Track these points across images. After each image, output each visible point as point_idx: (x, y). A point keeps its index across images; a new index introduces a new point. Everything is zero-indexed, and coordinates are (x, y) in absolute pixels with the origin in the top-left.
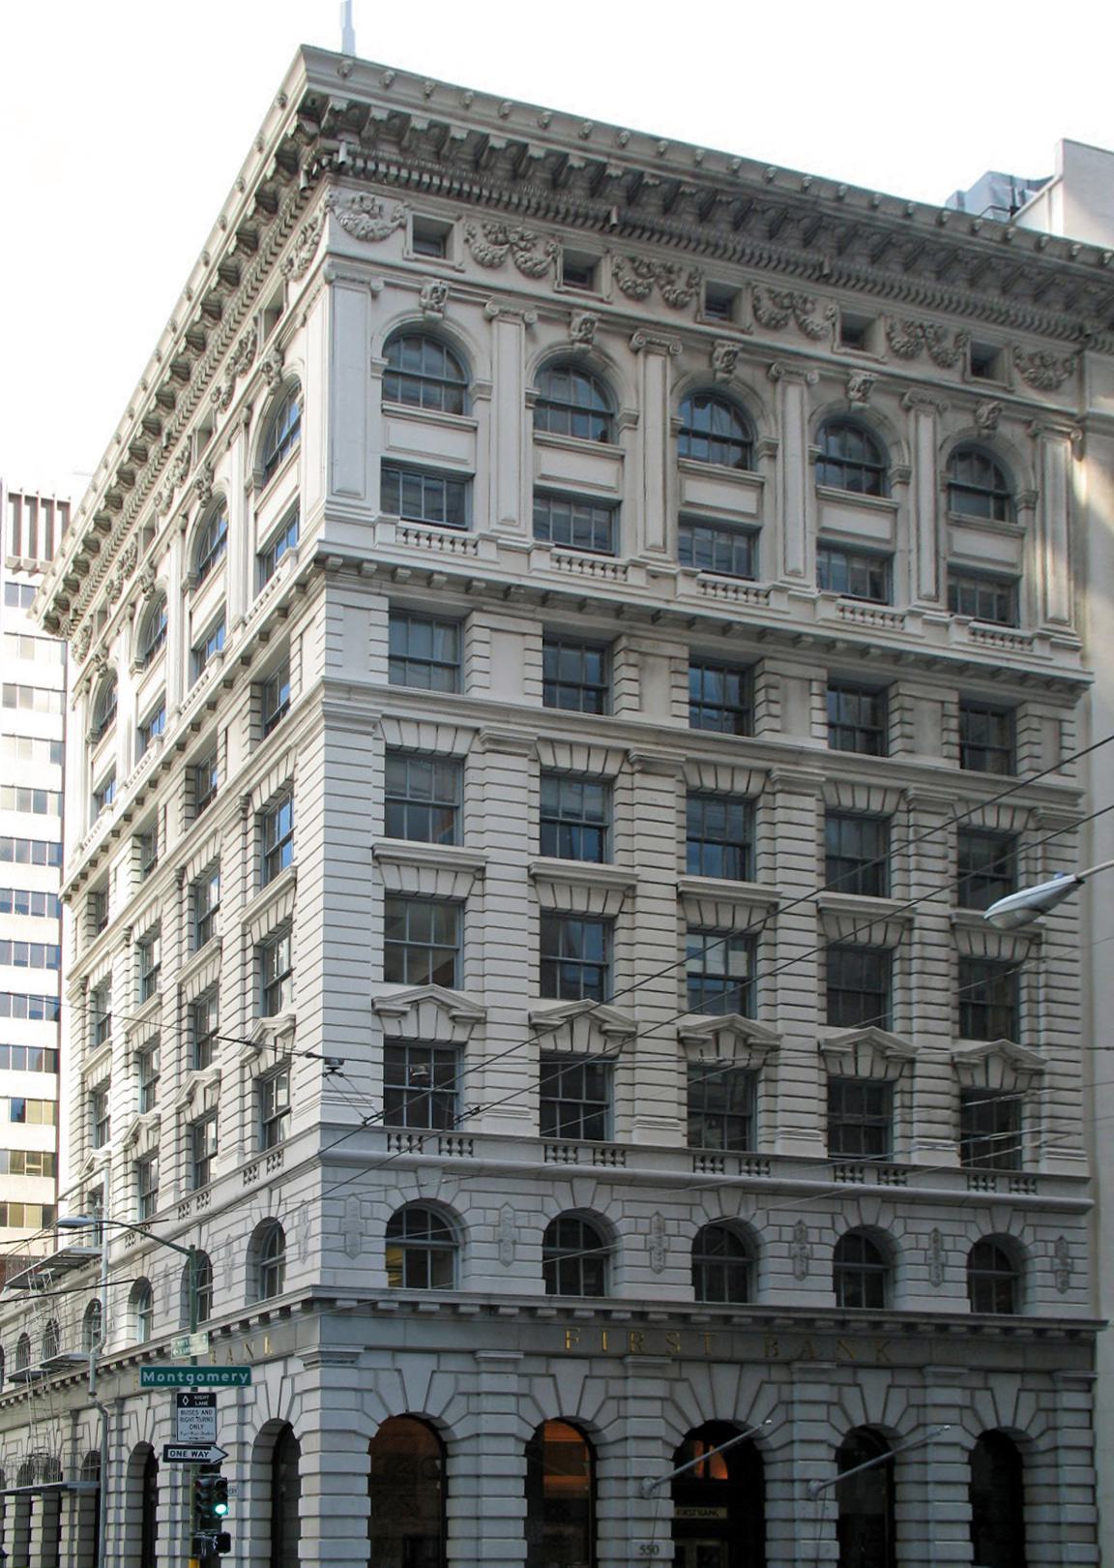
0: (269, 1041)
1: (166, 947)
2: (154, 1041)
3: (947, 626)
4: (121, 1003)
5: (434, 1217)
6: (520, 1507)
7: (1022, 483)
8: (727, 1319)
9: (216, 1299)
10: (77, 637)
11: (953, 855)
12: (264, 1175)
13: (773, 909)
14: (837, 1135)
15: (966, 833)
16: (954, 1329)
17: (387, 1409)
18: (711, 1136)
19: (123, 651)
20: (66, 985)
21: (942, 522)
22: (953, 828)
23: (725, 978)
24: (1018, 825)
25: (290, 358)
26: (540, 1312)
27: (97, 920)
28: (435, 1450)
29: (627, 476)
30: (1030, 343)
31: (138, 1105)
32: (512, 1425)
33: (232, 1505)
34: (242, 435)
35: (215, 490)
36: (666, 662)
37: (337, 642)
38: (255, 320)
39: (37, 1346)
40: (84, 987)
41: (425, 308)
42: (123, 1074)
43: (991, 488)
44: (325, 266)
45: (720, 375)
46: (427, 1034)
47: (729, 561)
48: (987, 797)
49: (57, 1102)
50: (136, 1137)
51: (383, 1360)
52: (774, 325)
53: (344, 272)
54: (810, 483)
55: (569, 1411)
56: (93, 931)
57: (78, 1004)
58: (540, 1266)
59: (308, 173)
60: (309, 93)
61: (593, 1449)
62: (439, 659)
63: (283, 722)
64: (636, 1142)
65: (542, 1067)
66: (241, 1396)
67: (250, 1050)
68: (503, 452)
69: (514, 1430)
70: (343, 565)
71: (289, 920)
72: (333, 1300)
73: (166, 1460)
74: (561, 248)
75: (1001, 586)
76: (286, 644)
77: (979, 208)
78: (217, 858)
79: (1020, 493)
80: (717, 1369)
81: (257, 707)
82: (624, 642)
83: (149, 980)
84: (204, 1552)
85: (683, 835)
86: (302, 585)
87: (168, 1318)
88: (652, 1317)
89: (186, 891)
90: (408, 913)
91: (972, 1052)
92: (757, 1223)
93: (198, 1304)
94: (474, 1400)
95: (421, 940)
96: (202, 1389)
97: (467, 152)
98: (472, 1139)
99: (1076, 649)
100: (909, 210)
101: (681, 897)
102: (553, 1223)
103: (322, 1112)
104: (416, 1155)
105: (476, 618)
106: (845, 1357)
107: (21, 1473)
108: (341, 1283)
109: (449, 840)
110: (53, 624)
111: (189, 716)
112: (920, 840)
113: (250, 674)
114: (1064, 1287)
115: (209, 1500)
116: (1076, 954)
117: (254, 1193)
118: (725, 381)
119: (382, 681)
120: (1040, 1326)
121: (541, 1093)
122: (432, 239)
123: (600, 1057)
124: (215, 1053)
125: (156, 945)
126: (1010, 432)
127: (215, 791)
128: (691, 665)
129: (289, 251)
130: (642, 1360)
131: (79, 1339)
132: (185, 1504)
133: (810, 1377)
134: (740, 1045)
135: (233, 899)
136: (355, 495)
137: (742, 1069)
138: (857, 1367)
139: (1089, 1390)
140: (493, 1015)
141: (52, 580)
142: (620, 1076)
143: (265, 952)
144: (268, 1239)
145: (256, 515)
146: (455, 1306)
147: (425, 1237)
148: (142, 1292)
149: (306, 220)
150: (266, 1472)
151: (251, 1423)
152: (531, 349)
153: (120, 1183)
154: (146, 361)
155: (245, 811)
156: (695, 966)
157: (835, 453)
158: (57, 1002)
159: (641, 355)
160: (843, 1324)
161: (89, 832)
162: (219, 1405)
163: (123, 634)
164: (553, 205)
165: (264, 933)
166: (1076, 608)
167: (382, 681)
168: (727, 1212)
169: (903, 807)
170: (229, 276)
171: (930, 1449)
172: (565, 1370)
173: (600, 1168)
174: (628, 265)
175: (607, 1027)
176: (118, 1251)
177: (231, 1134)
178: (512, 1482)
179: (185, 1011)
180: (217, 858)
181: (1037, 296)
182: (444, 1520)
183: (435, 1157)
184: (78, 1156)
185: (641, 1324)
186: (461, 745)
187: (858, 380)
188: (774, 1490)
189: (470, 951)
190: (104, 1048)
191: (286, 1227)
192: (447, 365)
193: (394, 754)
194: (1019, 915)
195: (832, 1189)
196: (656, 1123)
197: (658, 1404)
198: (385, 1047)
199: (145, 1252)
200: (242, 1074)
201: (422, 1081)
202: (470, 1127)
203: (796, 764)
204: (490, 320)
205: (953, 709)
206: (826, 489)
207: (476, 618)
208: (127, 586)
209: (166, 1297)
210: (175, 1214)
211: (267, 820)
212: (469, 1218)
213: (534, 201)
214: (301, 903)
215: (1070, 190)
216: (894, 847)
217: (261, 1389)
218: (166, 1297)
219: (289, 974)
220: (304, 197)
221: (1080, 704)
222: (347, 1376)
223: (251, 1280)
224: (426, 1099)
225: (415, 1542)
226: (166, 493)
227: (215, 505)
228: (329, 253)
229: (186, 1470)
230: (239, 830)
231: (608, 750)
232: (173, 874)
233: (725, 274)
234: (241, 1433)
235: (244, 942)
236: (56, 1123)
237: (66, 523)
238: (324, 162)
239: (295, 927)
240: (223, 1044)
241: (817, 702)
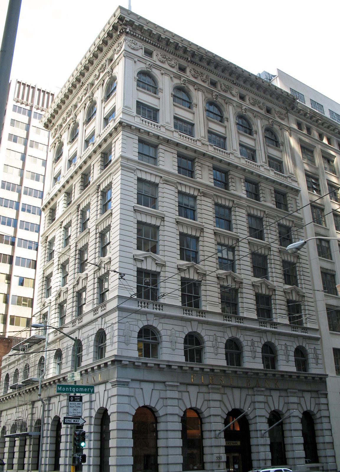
0: (103, 265)
1: (73, 230)
2: (67, 262)
3: (269, 170)
4: (58, 247)
5: (152, 332)
6: (180, 443)
7: (280, 140)
8: (236, 372)
9: (84, 358)
10: (53, 131)
11: (277, 231)
12: (100, 313)
13: (238, 240)
14: (259, 311)
15: (280, 225)
16: (293, 377)
17: (138, 404)
18: (227, 309)
19: (66, 137)
20: (41, 238)
21: (265, 145)
22: (276, 223)
23: (228, 260)
24: (291, 225)
25: (114, 71)
26: (184, 368)
27: (52, 218)
28: (153, 420)
29: (195, 118)
30: (278, 109)
31: (61, 283)
32: (176, 410)
33: (87, 442)
34: (101, 87)
35: (94, 99)
36: (207, 167)
37: (125, 146)
38: (106, 60)
39: (21, 374)
40: (46, 240)
41: (147, 68)
42: (57, 272)
43: (274, 139)
44: (123, 52)
45: (214, 99)
46: (149, 268)
47: (220, 144)
48: (283, 216)
49: (34, 280)
50: (59, 295)
51: (136, 385)
52: (225, 91)
53: (128, 55)
54: (236, 129)
55: (194, 406)
56: (50, 221)
57: (44, 246)
58: (183, 351)
59: (120, 32)
60: (120, 15)
61: (201, 419)
62: (151, 155)
63: (109, 165)
64: (208, 310)
65: (182, 283)
66: (91, 397)
67: (97, 268)
68: (167, 108)
69: (177, 412)
70: (126, 125)
71: (110, 225)
72: (121, 361)
73: (64, 423)
74: (178, 62)
75: (279, 163)
76: (111, 144)
77: (263, 77)
78: (89, 203)
79: (280, 142)
80: (234, 389)
81: (103, 160)
82: (197, 160)
83: (67, 240)
84: (77, 462)
85: (214, 216)
86: (116, 129)
87: (67, 367)
88: (215, 371)
89: (80, 212)
90: (144, 228)
91: (288, 289)
92: (241, 339)
93: (77, 360)
94: (165, 400)
95: (147, 237)
96: (78, 394)
97: (156, 37)
98: (163, 305)
99: (296, 182)
100: (250, 75)
101: (215, 234)
102: (186, 336)
103: (119, 292)
104: (146, 309)
105: (160, 146)
106: (267, 386)
107: (12, 428)
108: (124, 354)
109: (154, 207)
110: (46, 126)
111: (83, 159)
112: (270, 226)
113: (101, 150)
114: (317, 364)
115: (79, 440)
116: (307, 263)
117: (96, 319)
118: (215, 101)
119: (136, 159)
120: (313, 376)
121: (182, 291)
122: (149, 53)
123: (197, 281)
124: (86, 268)
125: (70, 228)
126: (276, 127)
127: (90, 182)
128: (213, 169)
129: (115, 47)
130: (214, 386)
131: (36, 372)
132: (71, 442)
133: (259, 393)
134: (233, 281)
135: (93, 215)
136: (130, 108)
137: (234, 289)
138: (271, 389)
139: (326, 397)
140: (168, 264)
141: (47, 114)
142: (203, 287)
143: (102, 235)
144: (101, 336)
145: (104, 108)
146: (159, 365)
147: (149, 339)
148: (59, 354)
149: (119, 41)
150: (98, 429)
152: (172, 83)
153: (53, 312)
155: (98, 190)
156: (220, 255)
157: (241, 123)
158: (37, 244)
159: (197, 90)
160: (266, 374)
161: (52, 189)
162: (83, 401)
163: (66, 132)
164: (176, 53)
165: (102, 229)
166: (295, 171)
167: (136, 159)
168: (233, 335)
169: (265, 216)
170: (100, 49)
171: (291, 418)
172: (193, 390)
173: (198, 318)
174: (193, 70)
175: (198, 271)
176: (51, 338)
177: (90, 296)
178: (178, 466)
179: (77, 252)
180: (89, 203)
181: (277, 99)
182: (157, 448)
183: (152, 310)
184: (40, 301)
185: (212, 373)
186: (157, 180)
187: (244, 108)
188: (253, 434)
189: (161, 243)
190: (51, 262)
191: (106, 332)
192: (152, 82)
193: (140, 180)
194: (294, 250)
195: (259, 329)
196: (213, 304)
197: (219, 403)
198: (137, 271)
199: (61, 339)
200: (94, 276)
201: (147, 284)
202: (162, 301)
203: (240, 200)
204: (162, 74)
205: (273, 192)
206: (240, 131)
207: (160, 146)
208: (68, 119)
210: (71, 325)
211: (104, 194)
212: (163, 333)
214: (113, 221)
215: (280, 79)
216: (264, 227)
217: (97, 394)
218: (67, 357)
219: (109, 243)
220: (119, 37)
221: (299, 195)
222: (125, 391)
223: (95, 352)
224: (149, 289)
225: (148, 457)
226: (80, 97)
227: (93, 103)
228: (124, 50)
229: (71, 428)
230: (96, 196)
231: (195, 188)
232: (76, 206)
233: (215, 78)
234: (90, 413)
235: (96, 231)
236: (34, 287)
237: (53, 99)
238: (124, 30)
239: (111, 228)
240: (89, 265)
241: (243, 184)
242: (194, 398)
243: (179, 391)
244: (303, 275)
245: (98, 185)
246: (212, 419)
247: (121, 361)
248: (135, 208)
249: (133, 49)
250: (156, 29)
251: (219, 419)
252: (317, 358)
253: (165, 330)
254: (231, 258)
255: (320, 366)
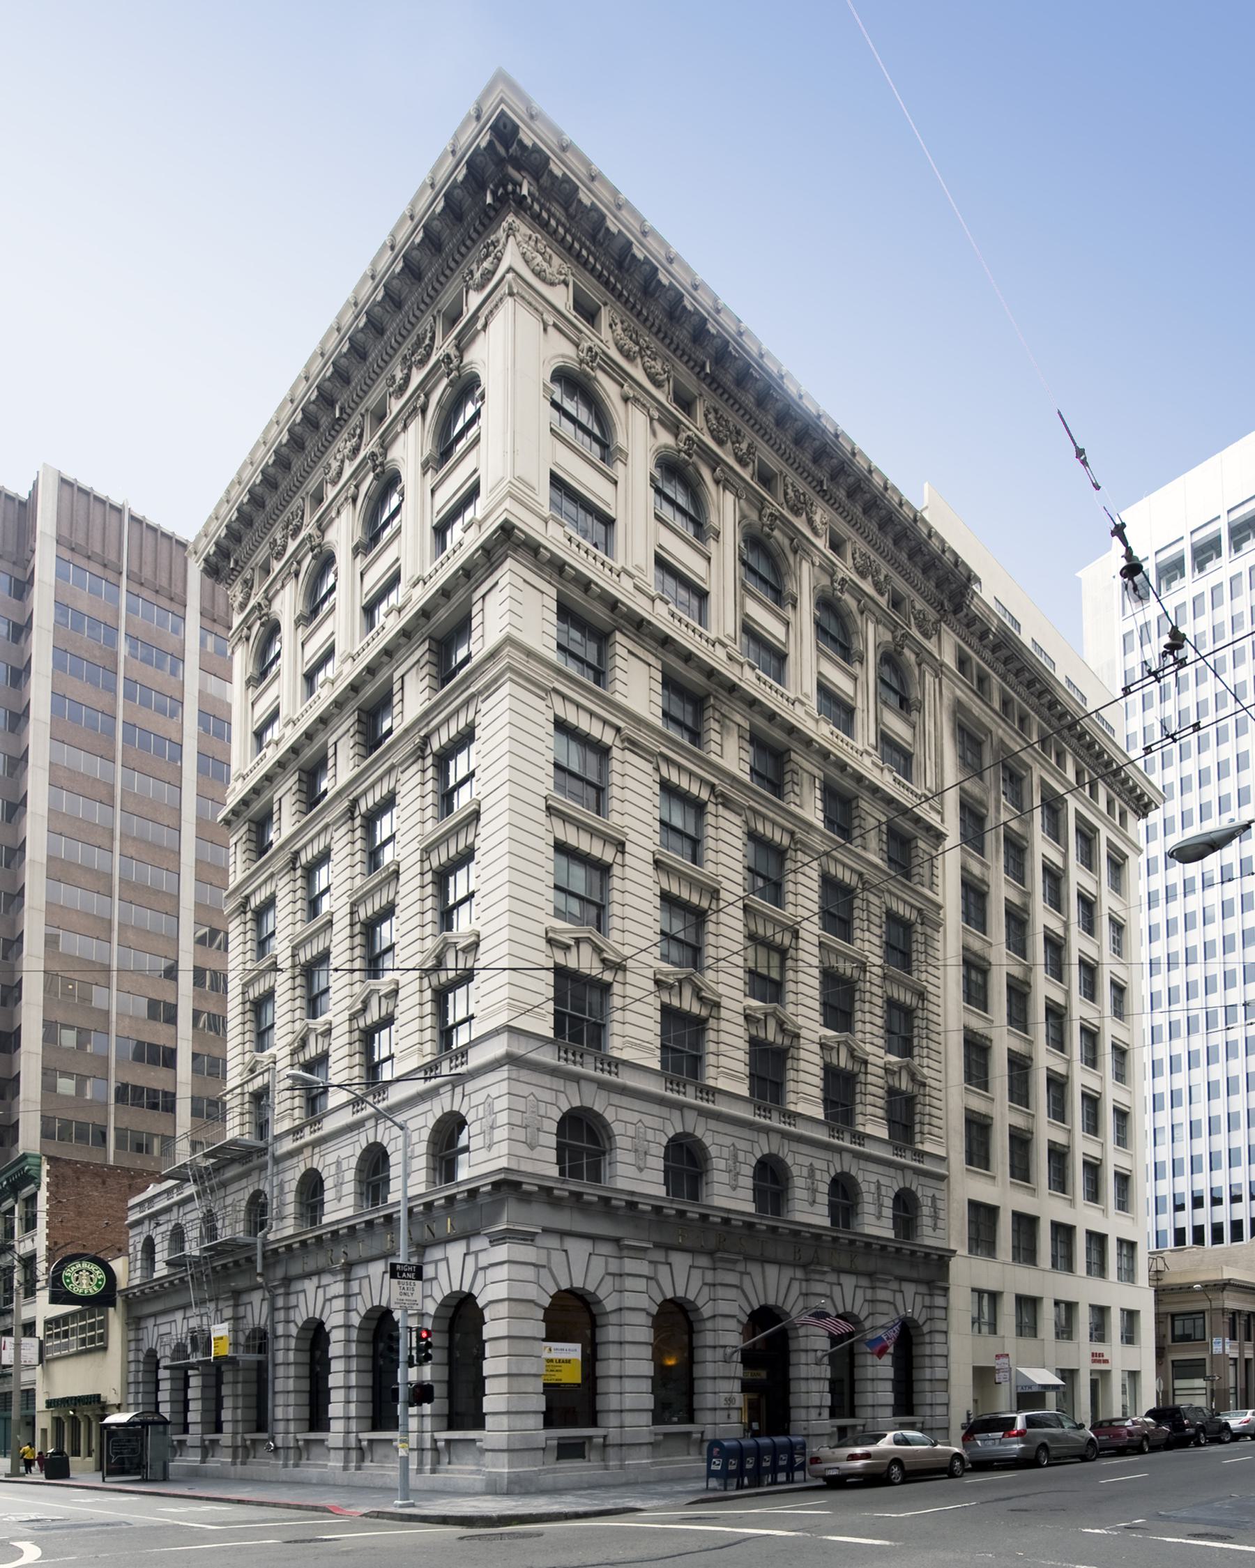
9: (327, 1208)
30: (920, 605)
34: (419, 418)
50: (304, 1043)
51: (553, 1242)
72: (520, 1184)
76: (469, 604)
104: (578, 1068)
136: (532, 489)
150: (305, 1358)
151: (294, 1321)
154: (462, 116)
179: (357, 928)
181: (925, 571)
183: (591, 1072)
186: (608, 737)
196: (732, 1075)
207: (618, 636)
208: (292, 546)
209: (339, 1185)
213: (657, 322)
214: (403, 891)
217: (442, 1265)
218: (339, 1185)
223: (360, 1194)
234: (347, 1318)
238: (510, 187)
242: (683, 1277)
243: (650, 1262)
244: (927, 1038)
245: (422, 734)
246: (721, 1323)
247: (518, 1184)
248: (550, 802)
249: (538, 274)
250: (618, 214)
251: (732, 1324)
252: (935, 1217)
253: (623, 1120)
254: (775, 975)
255: (939, 1233)
